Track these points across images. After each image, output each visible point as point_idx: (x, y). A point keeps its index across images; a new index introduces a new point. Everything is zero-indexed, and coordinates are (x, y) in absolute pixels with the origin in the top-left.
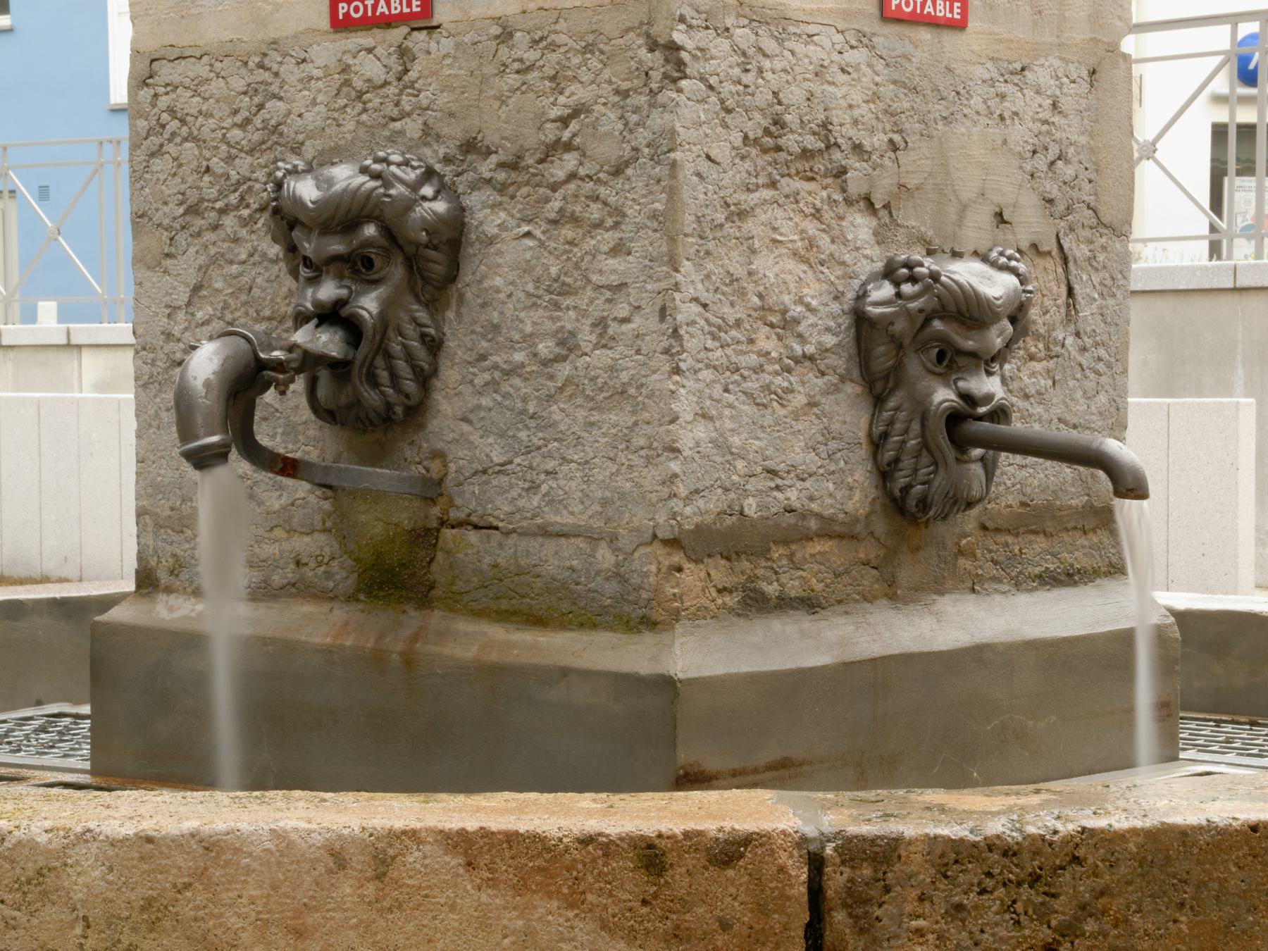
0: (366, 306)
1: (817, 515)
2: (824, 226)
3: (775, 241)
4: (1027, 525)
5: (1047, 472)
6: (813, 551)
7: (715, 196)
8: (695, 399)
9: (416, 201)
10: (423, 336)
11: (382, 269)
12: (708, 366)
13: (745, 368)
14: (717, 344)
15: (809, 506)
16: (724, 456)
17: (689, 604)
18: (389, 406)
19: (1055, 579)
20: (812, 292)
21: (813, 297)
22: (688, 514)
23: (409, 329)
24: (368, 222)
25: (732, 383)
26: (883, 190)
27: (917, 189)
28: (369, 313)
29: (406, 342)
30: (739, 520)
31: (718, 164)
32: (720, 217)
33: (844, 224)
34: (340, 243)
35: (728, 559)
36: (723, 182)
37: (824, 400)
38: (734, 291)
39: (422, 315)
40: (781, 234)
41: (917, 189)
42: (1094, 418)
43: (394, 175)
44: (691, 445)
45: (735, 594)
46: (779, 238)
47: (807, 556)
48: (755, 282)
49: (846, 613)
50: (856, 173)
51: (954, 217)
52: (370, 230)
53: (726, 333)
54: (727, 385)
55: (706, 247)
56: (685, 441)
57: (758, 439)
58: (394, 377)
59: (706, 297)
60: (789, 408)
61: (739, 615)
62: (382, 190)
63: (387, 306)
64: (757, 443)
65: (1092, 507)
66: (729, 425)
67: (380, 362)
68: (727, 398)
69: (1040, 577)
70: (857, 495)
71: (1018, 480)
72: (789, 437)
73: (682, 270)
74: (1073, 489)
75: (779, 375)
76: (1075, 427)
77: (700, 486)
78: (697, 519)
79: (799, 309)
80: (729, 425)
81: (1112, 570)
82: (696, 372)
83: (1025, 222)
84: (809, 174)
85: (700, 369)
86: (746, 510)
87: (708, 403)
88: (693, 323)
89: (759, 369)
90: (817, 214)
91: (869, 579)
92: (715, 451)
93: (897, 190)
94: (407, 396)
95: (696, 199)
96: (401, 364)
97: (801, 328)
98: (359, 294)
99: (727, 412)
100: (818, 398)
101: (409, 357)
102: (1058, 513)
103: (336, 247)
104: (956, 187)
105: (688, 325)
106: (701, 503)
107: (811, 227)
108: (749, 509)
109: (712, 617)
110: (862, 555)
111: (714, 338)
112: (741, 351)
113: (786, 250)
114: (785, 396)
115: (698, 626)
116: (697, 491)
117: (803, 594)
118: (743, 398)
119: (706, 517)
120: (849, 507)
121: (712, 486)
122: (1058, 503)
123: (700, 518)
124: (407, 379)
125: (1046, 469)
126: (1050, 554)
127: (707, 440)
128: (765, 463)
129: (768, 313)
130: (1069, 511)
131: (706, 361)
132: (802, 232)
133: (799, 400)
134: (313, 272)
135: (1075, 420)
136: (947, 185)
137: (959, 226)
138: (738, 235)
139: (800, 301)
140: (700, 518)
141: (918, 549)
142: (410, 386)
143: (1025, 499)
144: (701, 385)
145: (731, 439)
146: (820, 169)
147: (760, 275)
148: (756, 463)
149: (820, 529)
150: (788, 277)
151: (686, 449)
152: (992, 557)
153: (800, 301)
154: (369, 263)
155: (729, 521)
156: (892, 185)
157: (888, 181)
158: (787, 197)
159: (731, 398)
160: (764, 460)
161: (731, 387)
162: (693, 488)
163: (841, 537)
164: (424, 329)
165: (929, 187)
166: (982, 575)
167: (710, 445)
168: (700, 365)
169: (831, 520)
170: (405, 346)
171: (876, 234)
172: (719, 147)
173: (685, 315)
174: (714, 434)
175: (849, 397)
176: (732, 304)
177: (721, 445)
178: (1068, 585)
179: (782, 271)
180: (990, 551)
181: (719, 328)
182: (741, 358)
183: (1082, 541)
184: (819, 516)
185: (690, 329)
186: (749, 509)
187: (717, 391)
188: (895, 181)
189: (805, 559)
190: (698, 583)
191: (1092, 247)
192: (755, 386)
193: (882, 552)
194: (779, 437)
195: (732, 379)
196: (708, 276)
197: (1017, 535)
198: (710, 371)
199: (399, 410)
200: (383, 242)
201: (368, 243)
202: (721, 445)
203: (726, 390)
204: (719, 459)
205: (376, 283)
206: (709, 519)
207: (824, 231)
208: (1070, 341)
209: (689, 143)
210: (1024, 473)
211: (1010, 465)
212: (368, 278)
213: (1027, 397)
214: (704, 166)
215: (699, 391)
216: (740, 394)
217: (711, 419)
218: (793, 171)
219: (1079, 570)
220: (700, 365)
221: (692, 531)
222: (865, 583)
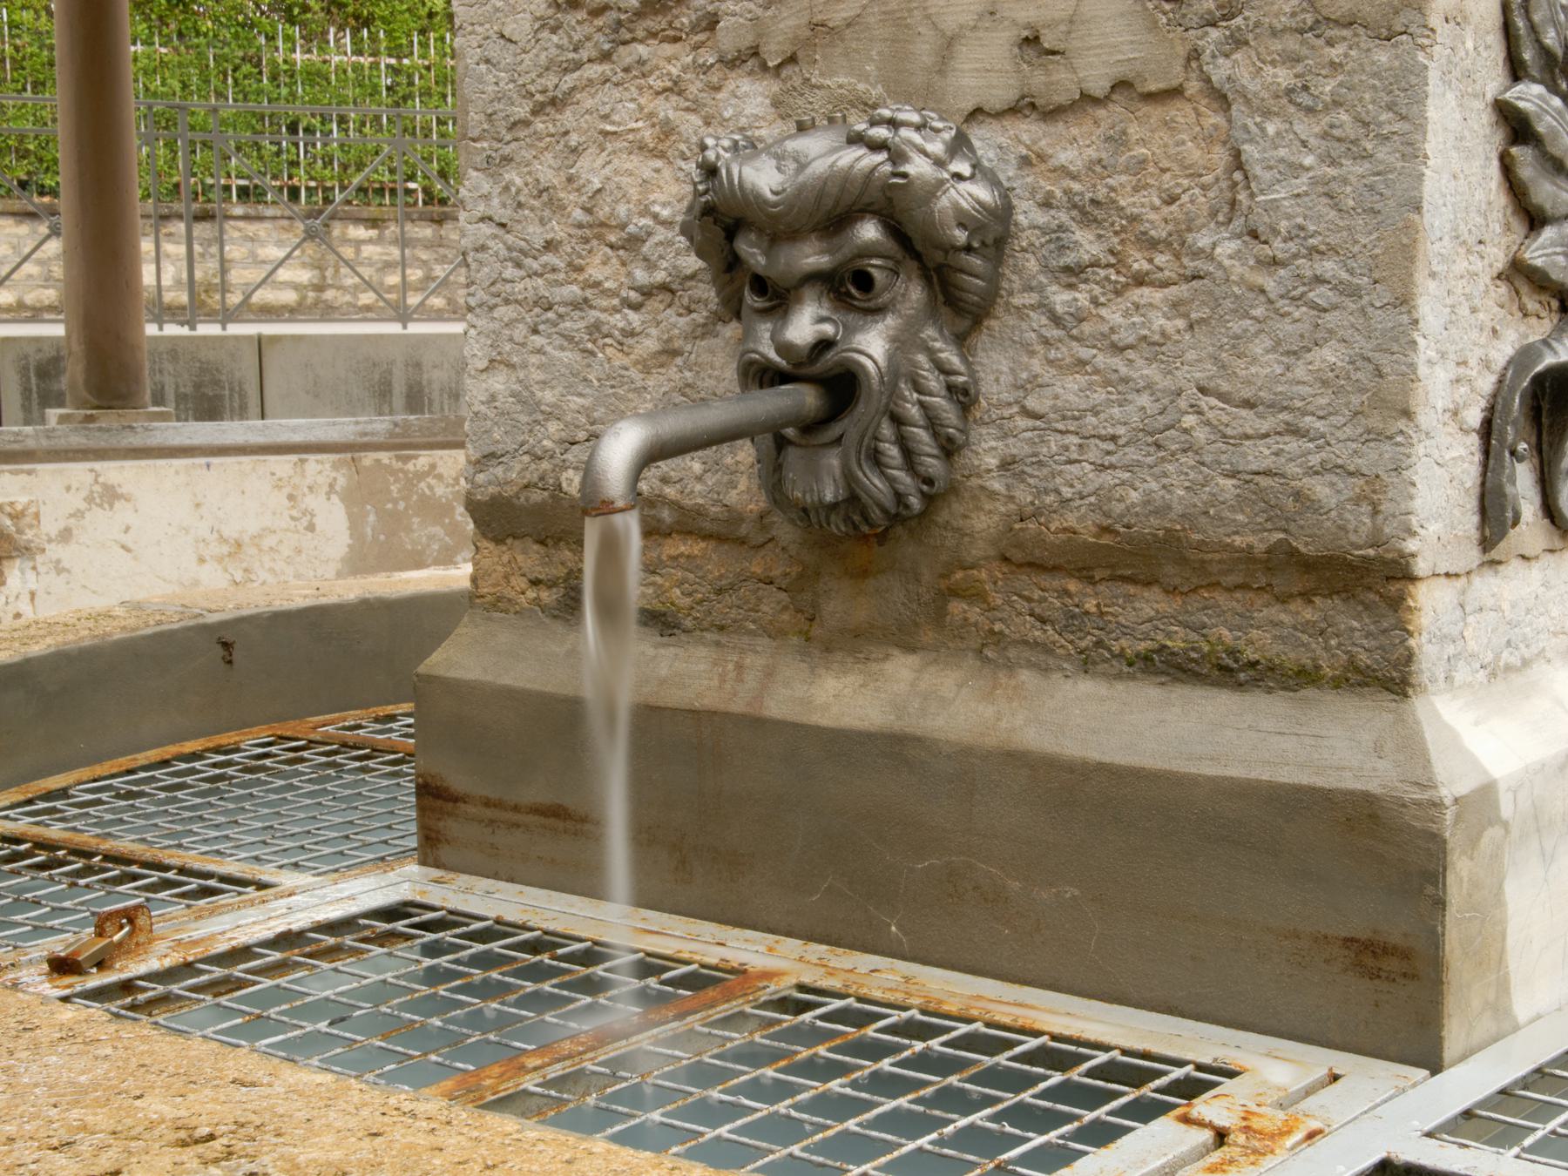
0: (871, 351)
1: (672, 502)
2: (687, 104)
3: (606, 134)
4: (1112, 567)
5: (1165, 481)
6: (673, 552)
7: (511, 86)
8: (489, 342)
9: (941, 182)
10: (950, 388)
11: (885, 289)
12: (507, 302)
13: (559, 304)
14: (523, 273)
15: (661, 490)
16: (530, 415)
17: (486, 590)
18: (899, 497)
19: (1179, 668)
20: (662, 198)
21: (664, 205)
22: (481, 482)
23: (934, 382)
24: (862, 219)
25: (543, 322)
26: (780, 38)
27: (849, 25)
28: (875, 362)
29: (923, 398)
30: (553, 497)
31: (515, 43)
32: (522, 110)
33: (719, 96)
34: (822, 252)
35: (542, 543)
36: (524, 65)
37: (688, 347)
38: (545, 204)
39: (951, 357)
40: (613, 123)
41: (849, 25)
42: (1304, 390)
43: (910, 142)
44: (484, 399)
45: (555, 590)
46: (609, 128)
47: (664, 558)
48: (578, 190)
49: (718, 644)
50: (733, 19)
51: (928, 60)
52: (869, 231)
53: (535, 258)
54: (536, 324)
55: (501, 152)
56: (475, 393)
57: (580, 395)
58: (909, 454)
59: (503, 214)
60: (632, 356)
61: (555, 617)
62: (888, 168)
63: (901, 344)
64: (579, 400)
65: (1293, 553)
66: (537, 375)
67: (887, 430)
68: (533, 342)
69: (1146, 658)
70: (743, 484)
71: (1091, 488)
72: (630, 396)
73: (466, 183)
74: (1240, 517)
75: (618, 311)
76: (1248, 404)
77: (499, 449)
78: (491, 490)
79: (643, 221)
80: (537, 375)
81: (1354, 677)
82: (492, 308)
83: (1100, 46)
84: (671, 33)
85: (496, 306)
86: (564, 485)
87: (508, 347)
88: (483, 248)
89: (581, 305)
90: (675, 88)
91: (771, 604)
92: (519, 408)
93: (808, 33)
94: (929, 481)
95: (483, 93)
96: (922, 435)
97: (645, 249)
98: (850, 331)
99: (534, 359)
100: (677, 344)
101: (932, 422)
102: (1192, 555)
103: (811, 260)
104: (930, 11)
105: (477, 250)
106: (499, 471)
107: (666, 108)
108: (569, 485)
109: (516, 613)
110: (758, 570)
111: (518, 265)
112: (556, 281)
113: (625, 144)
114: (625, 340)
115: (489, 619)
116: (492, 455)
117: (659, 607)
118: (559, 341)
119: (508, 488)
120: (732, 497)
121: (516, 450)
122: (1196, 537)
123: (499, 489)
124: (929, 455)
125: (1165, 475)
126: (1181, 623)
127: (506, 394)
128: (594, 427)
129: (604, 230)
130: (1225, 556)
131: (503, 295)
132: (651, 115)
133: (650, 344)
134: (770, 300)
135: (1247, 393)
136: (910, 10)
137: (940, 72)
138: (552, 130)
139: (645, 212)
140: (499, 489)
141: (864, 573)
142: (932, 464)
143: (1107, 522)
144: (496, 325)
145: (539, 394)
146: (683, 24)
147: (581, 182)
148: (577, 427)
149: (678, 522)
150: (625, 180)
151: (476, 403)
152: (1032, 609)
153: (645, 212)
154: (864, 281)
155: (537, 496)
156: (798, 27)
157: (792, 22)
158: (626, 70)
159: (538, 341)
160: (592, 424)
161: (541, 327)
162: (487, 450)
163: (720, 538)
164: (953, 378)
165: (872, 20)
166: (1001, 633)
167: (511, 400)
168: (494, 301)
169: (699, 512)
170: (922, 405)
171: (776, 103)
172: (515, 21)
173: (472, 238)
174: (517, 387)
175: (727, 343)
176: (542, 222)
177: (525, 399)
178: (1216, 684)
179: (616, 172)
180: (1029, 600)
181: (521, 251)
182: (556, 290)
183: (1275, 612)
184: (676, 506)
185: (479, 256)
186: (569, 485)
187: (520, 332)
188: (804, 21)
189: (661, 561)
190: (499, 568)
191: (1299, 69)
192: (576, 327)
193: (795, 570)
194: (614, 394)
195: (544, 318)
196: (506, 189)
197: (1091, 581)
198: (511, 307)
199: (915, 502)
200: (891, 246)
201: (868, 251)
202: (525, 399)
203: (535, 331)
204: (524, 418)
205: (878, 311)
206: (509, 491)
207: (687, 109)
208: (1226, 248)
209: (473, 24)
210: (1108, 478)
211: (1070, 462)
212: (865, 305)
213: (1117, 349)
214: (495, 50)
215: (494, 332)
216: (555, 336)
217: (511, 366)
218: (640, 34)
219: (1253, 664)
220: (498, 300)
221: (486, 503)
222: (765, 608)
